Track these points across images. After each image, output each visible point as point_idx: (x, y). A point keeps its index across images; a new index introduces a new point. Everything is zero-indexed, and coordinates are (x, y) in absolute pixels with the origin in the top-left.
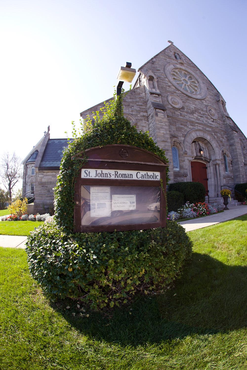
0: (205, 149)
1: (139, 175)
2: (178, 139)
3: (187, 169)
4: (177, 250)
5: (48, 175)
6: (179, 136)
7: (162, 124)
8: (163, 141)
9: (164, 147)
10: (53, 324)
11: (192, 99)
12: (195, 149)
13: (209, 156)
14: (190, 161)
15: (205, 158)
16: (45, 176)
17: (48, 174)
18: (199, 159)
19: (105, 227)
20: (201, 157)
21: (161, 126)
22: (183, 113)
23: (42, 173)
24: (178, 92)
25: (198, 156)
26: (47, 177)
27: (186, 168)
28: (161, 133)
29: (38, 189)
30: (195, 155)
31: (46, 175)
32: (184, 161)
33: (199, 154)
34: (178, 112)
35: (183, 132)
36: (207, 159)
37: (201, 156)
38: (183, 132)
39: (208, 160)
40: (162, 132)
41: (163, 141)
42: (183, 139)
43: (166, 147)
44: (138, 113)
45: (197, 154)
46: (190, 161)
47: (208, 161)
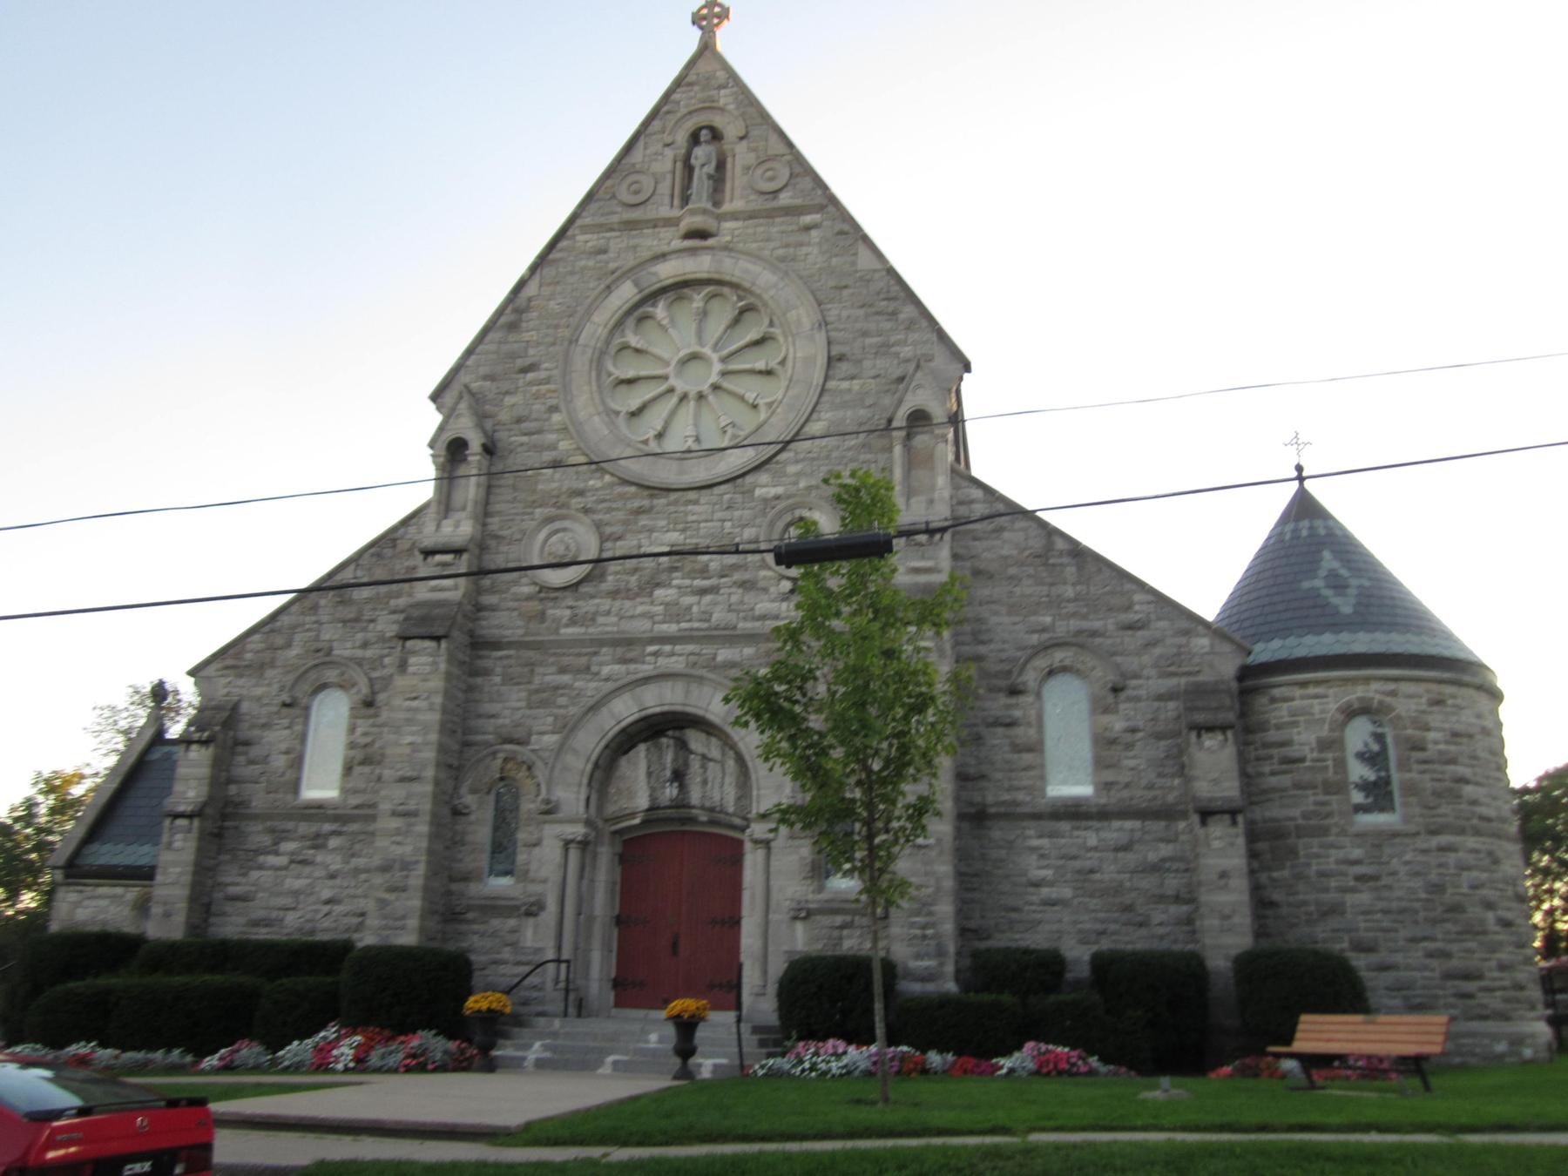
3: (545, 881)
4: (922, 959)
5: (100, 897)
6: (535, 729)
7: (415, 704)
8: (403, 780)
9: (401, 804)
10: (896, 883)
11: (673, 496)
13: (739, 799)
15: (712, 810)
17: (102, 890)
19: (1376, 571)
20: (682, 810)
21: (408, 715)
24: (599, 484)
25: (658, 808)
27: (543, 873)
28: (401, 745)
34: (564, 604)
35: (560, 707)
36: (727, 814)
38: (560, 707)
40: (409, 739)
41: (403, 780)
42: (551, 740)
43: (413, 802)
44: (386, 651)
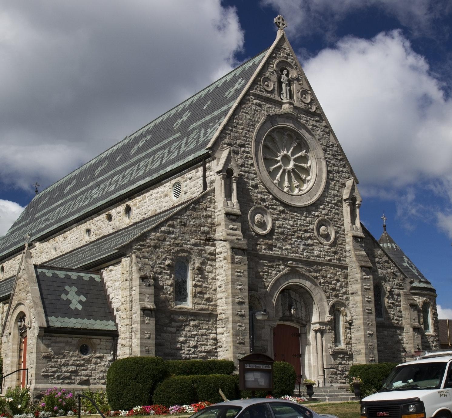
0: (300, 303)
1: (263, 367)
2: (257, 291)
3: (267, 341)
12: (282, 305)
13: (306, 315)
14: (271, 327)
16: (53, 342)
17: (59, 339)
18: (287, 320)
22: (312, 364)
23: (49, 338)
26: (57, 345)
29: (41, 365)
30: (281, 315)
31: (56, 342)
32: (263, 328)
33: (287, 313)
37: (291, 315)
39: (304, 323)
45: (283, 313)
46: (271, 327)
47: (303, 324)
